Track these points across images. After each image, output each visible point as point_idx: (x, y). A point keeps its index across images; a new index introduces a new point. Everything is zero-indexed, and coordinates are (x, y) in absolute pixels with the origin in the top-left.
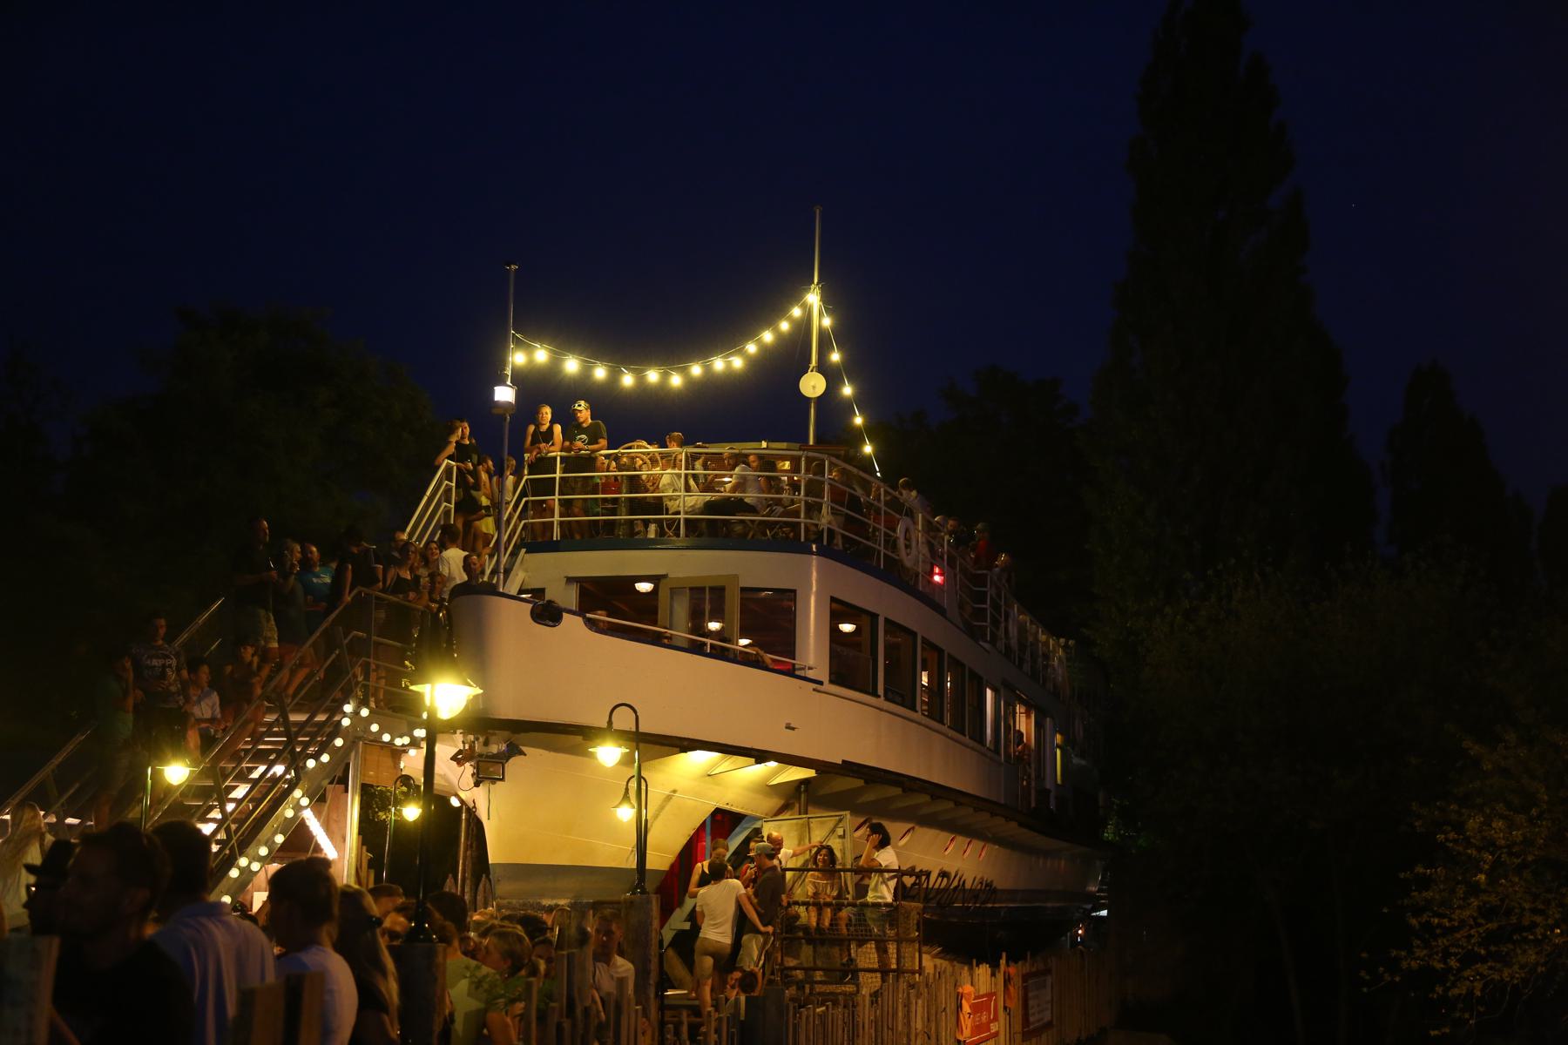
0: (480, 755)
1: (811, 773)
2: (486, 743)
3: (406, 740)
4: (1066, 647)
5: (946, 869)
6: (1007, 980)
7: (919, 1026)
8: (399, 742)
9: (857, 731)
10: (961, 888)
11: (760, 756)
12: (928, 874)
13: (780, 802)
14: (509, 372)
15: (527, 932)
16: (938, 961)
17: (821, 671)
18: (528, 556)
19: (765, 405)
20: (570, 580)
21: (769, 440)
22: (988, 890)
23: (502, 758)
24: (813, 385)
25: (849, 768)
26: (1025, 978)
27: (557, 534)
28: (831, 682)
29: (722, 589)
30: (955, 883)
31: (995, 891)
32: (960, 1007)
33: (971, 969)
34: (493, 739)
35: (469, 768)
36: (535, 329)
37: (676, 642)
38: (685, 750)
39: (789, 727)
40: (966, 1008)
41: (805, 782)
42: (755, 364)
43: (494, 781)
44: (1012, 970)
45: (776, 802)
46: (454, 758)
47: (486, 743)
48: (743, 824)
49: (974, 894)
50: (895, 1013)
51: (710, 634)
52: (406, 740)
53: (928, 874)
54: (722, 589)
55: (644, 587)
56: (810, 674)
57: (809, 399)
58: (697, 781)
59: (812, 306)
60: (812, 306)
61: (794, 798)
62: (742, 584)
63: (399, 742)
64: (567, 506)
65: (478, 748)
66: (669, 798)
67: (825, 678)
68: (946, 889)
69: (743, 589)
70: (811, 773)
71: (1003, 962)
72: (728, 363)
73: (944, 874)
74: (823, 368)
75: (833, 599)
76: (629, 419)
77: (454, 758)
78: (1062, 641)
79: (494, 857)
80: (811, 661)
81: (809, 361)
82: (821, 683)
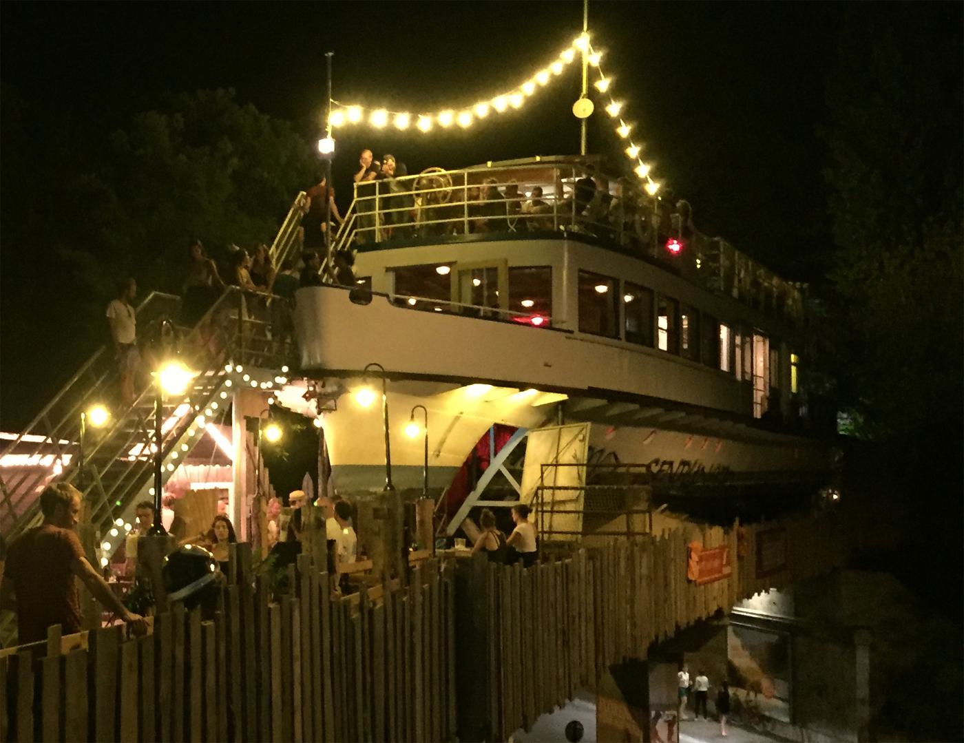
0: (320, 394)
1: (564, 397)
2: (323, 386)
3: (270, 384)
4: (801, 291)
5: (687, 458)
6: (740, 538)
7: (644, 571)
8: (264, 386)
9: (609, 366)
10: (701, 471)
11: (522, 386)
12: (671, 464)
13: (544, 418)
14: (329, 129)
15: (59, 526)
16: (685, 523)
17: (573, 325)
18: (359, 254)
19: (548, 130)
20: (388, 270)
21: (494, 160)
22: (725, 472)
23: (336, 395)
24: (583, 109)
25: (593, 392)
26: (759, 535)
27: (378, 239)
28: (581, 330)
29: (495, 269)
30: (696, 469)
31: (732, 473)
32: (689, 557)
33: (702, 530)
34: (327, 384)
35: (313, 402)
36: (345, 92)
37: (453, 310)
38: (464, 384)
39: (546, 365)
40: (695, 557)
41: (562, 403)
42: (529, 101)
43: (330, 410)
44: (743, 530)
45: (541, 418)
46: (304, 396)
47: (323, 386)
48: (517, 433)
49: (711, 476)
50: (616, 565)
51: (270, 325)
52: (270, 384)
53: (671, 464)
54: (495, 269)
55: (443, 270)
56: (565, 327)
57: (579, 120)
58: (476, 407)
59: (582, 49)
60: (582, 49)
61: (551, 416)
62: (510, 264)
63: (264, 386)
64: (387, 219)
65: (318, 389)
66: (457, 418)
67: (576, 329)
68: (688, 474)
69: (511, 269)
70: (564, 397)
71: (737, 523)
72: (511, 100)
73: (684, 463)
74: (593, 94)
75: (580, 270)
76: (415, 154)
77: (304, 396)
78: (798, 284)
79: (331, 464)
80: (564, 317)
81: (581, 90)
82: (571, 332)
